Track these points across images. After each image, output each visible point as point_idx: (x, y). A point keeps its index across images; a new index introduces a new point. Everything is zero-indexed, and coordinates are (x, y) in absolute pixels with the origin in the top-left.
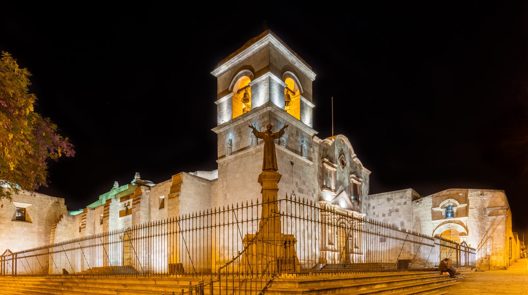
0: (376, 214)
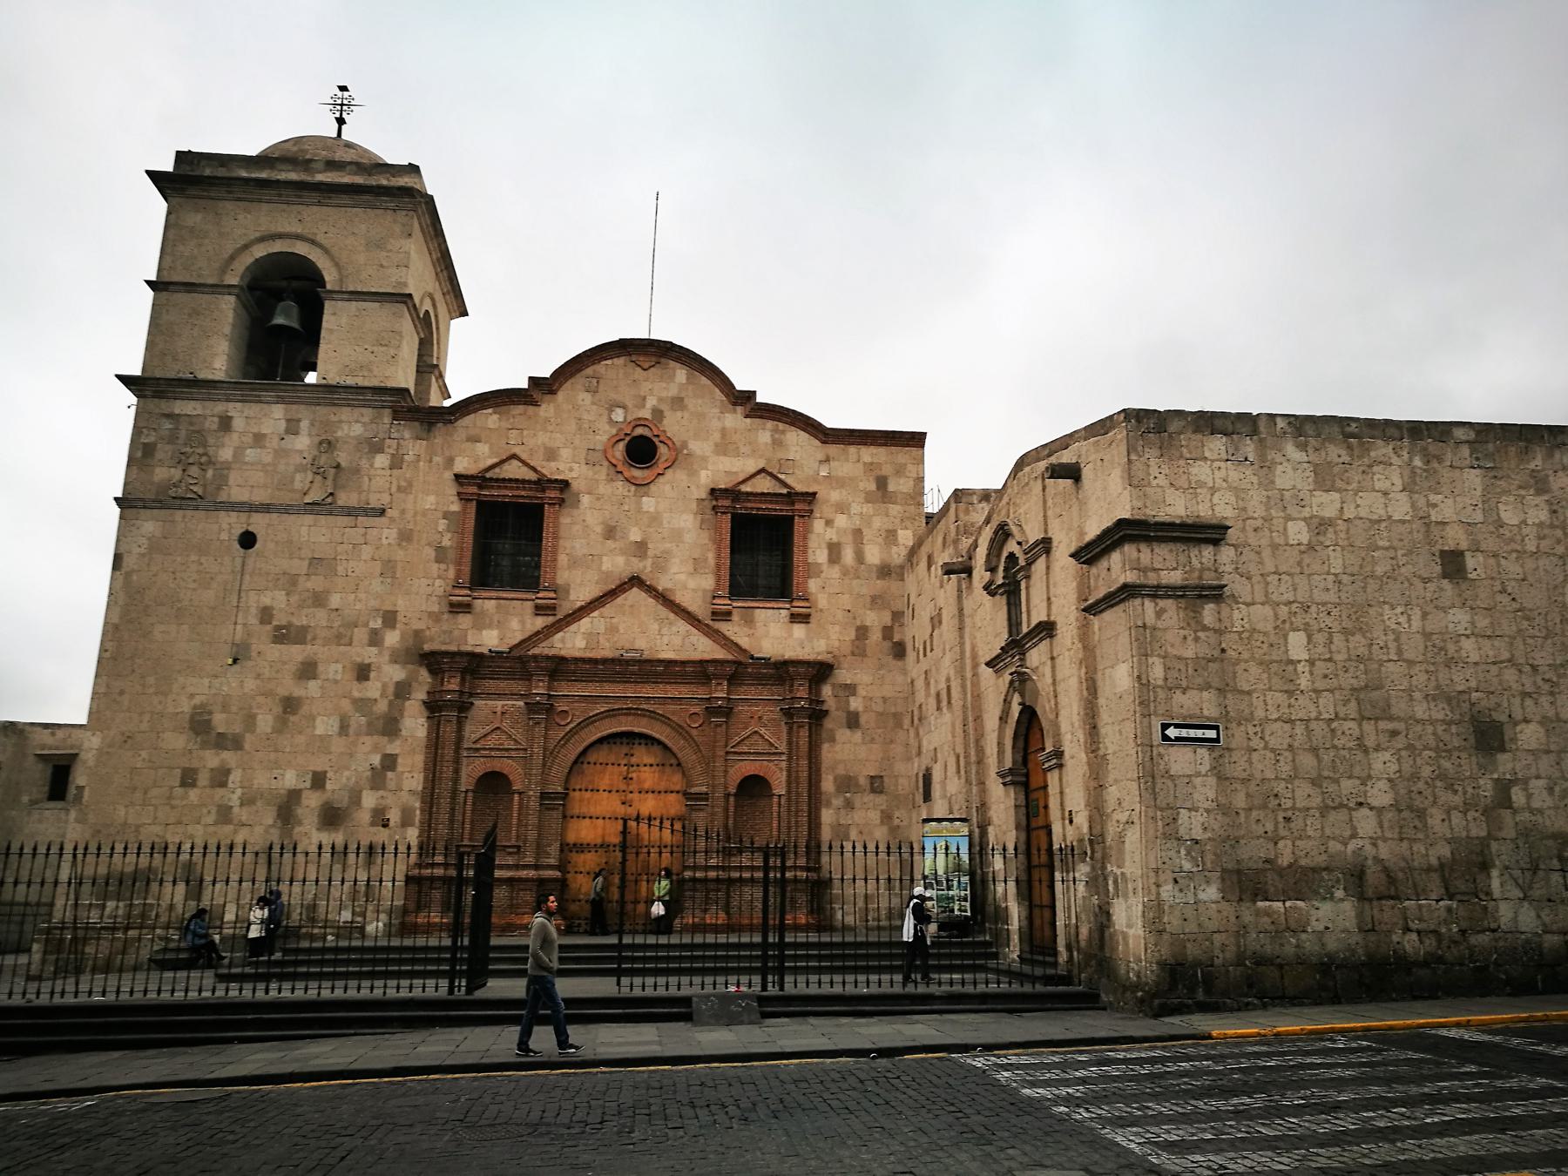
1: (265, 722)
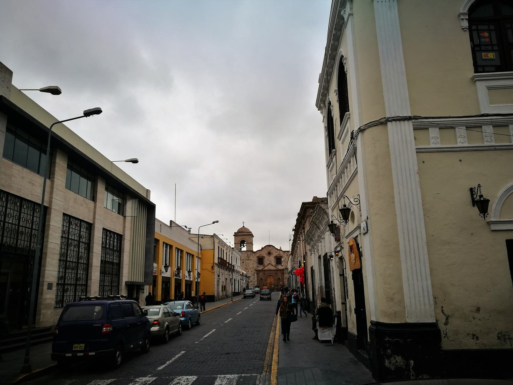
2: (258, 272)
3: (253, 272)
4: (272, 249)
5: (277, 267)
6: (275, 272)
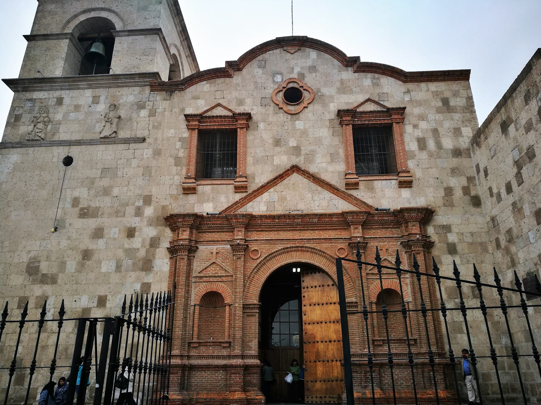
0: (495, 191)
1: (71, 266)
2: (185, 235)
3: (137, 242)
4: (313, 69)
5: (361, 194)
6: (344, 234)
